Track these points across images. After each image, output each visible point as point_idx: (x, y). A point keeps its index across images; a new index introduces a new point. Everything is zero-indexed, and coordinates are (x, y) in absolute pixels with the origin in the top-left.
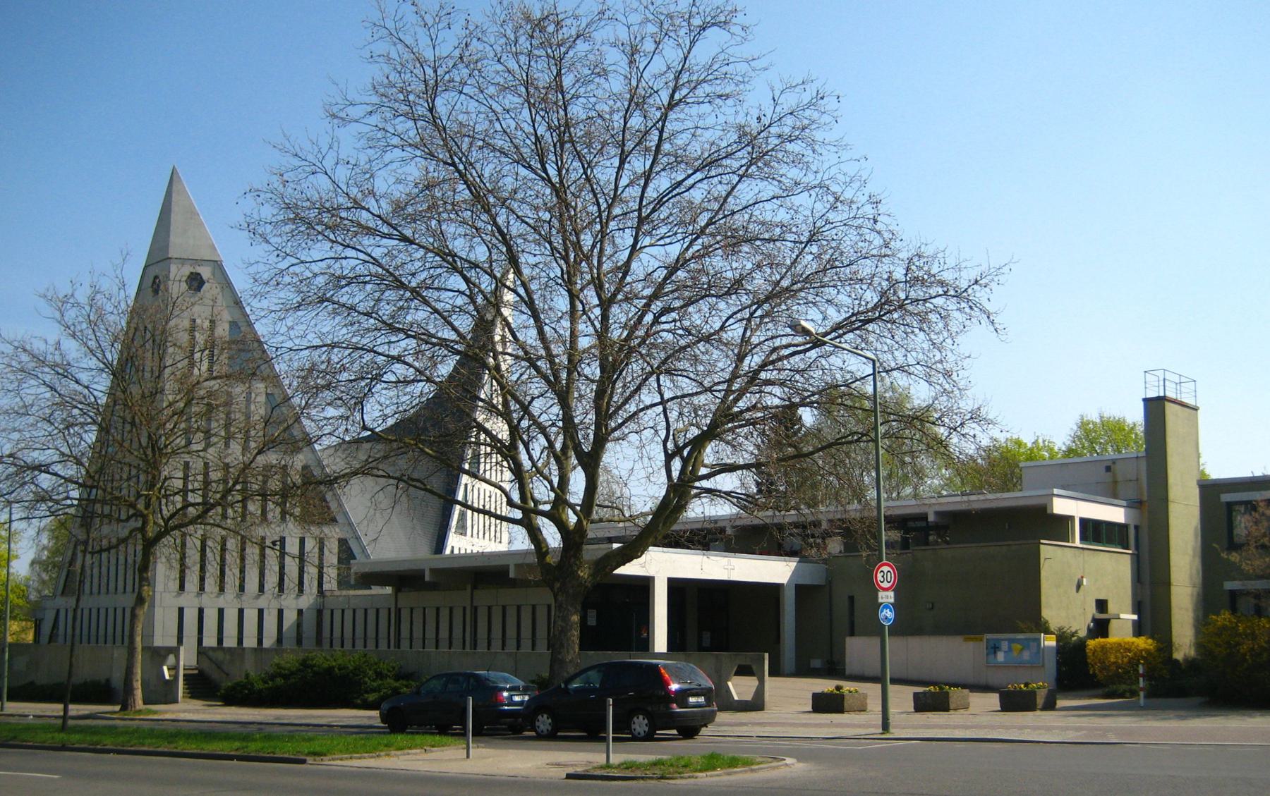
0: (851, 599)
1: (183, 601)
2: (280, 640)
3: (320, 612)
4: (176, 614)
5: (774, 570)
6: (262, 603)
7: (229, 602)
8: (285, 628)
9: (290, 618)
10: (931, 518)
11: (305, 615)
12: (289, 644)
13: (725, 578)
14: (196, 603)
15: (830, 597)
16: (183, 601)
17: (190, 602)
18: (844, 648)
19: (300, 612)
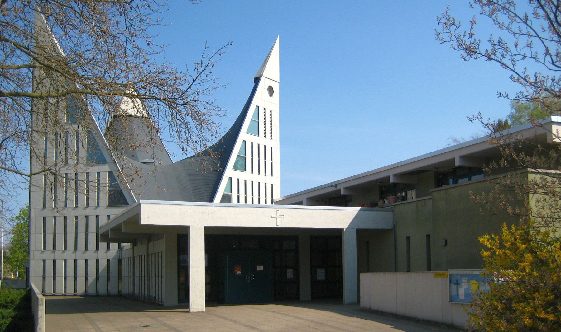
0: (408, 238)
1: (45, 256)
2: (97, 278)
3: (120, 261)
4: (424, 242)
5: (339, 218)
6: (87, 256)
7: (70, 255)
8: (100, 271)
9: (103, 264)
10: (457, 163)
11: (123, 262)
12: (103, 280)
13: (274, 225)
14: (74, 256)
15: (395, 243)
16: (45, 256)
17: (49, 256)
18: (280, 130)
19: (108, 260)
